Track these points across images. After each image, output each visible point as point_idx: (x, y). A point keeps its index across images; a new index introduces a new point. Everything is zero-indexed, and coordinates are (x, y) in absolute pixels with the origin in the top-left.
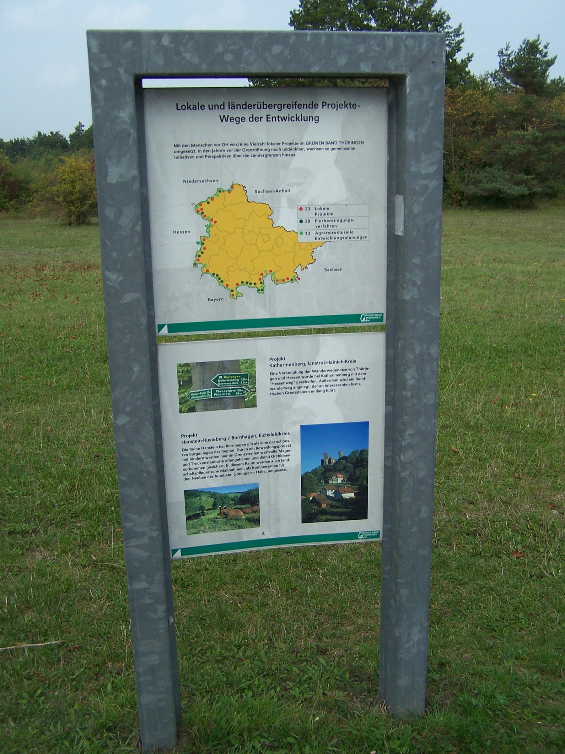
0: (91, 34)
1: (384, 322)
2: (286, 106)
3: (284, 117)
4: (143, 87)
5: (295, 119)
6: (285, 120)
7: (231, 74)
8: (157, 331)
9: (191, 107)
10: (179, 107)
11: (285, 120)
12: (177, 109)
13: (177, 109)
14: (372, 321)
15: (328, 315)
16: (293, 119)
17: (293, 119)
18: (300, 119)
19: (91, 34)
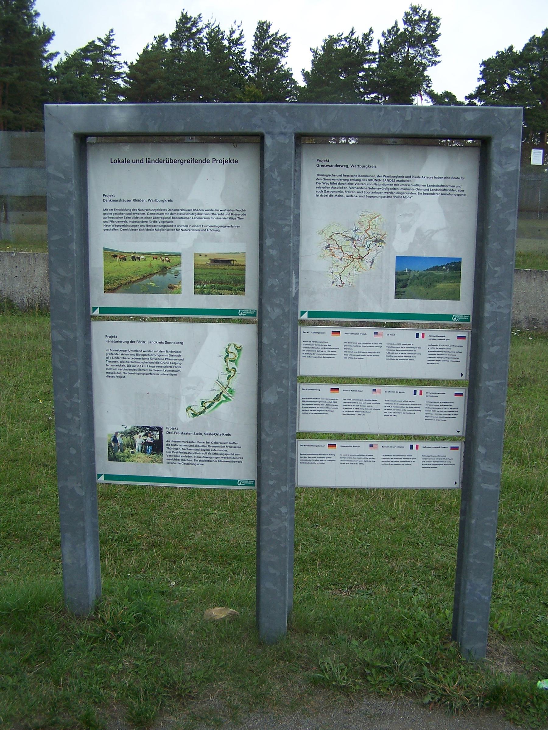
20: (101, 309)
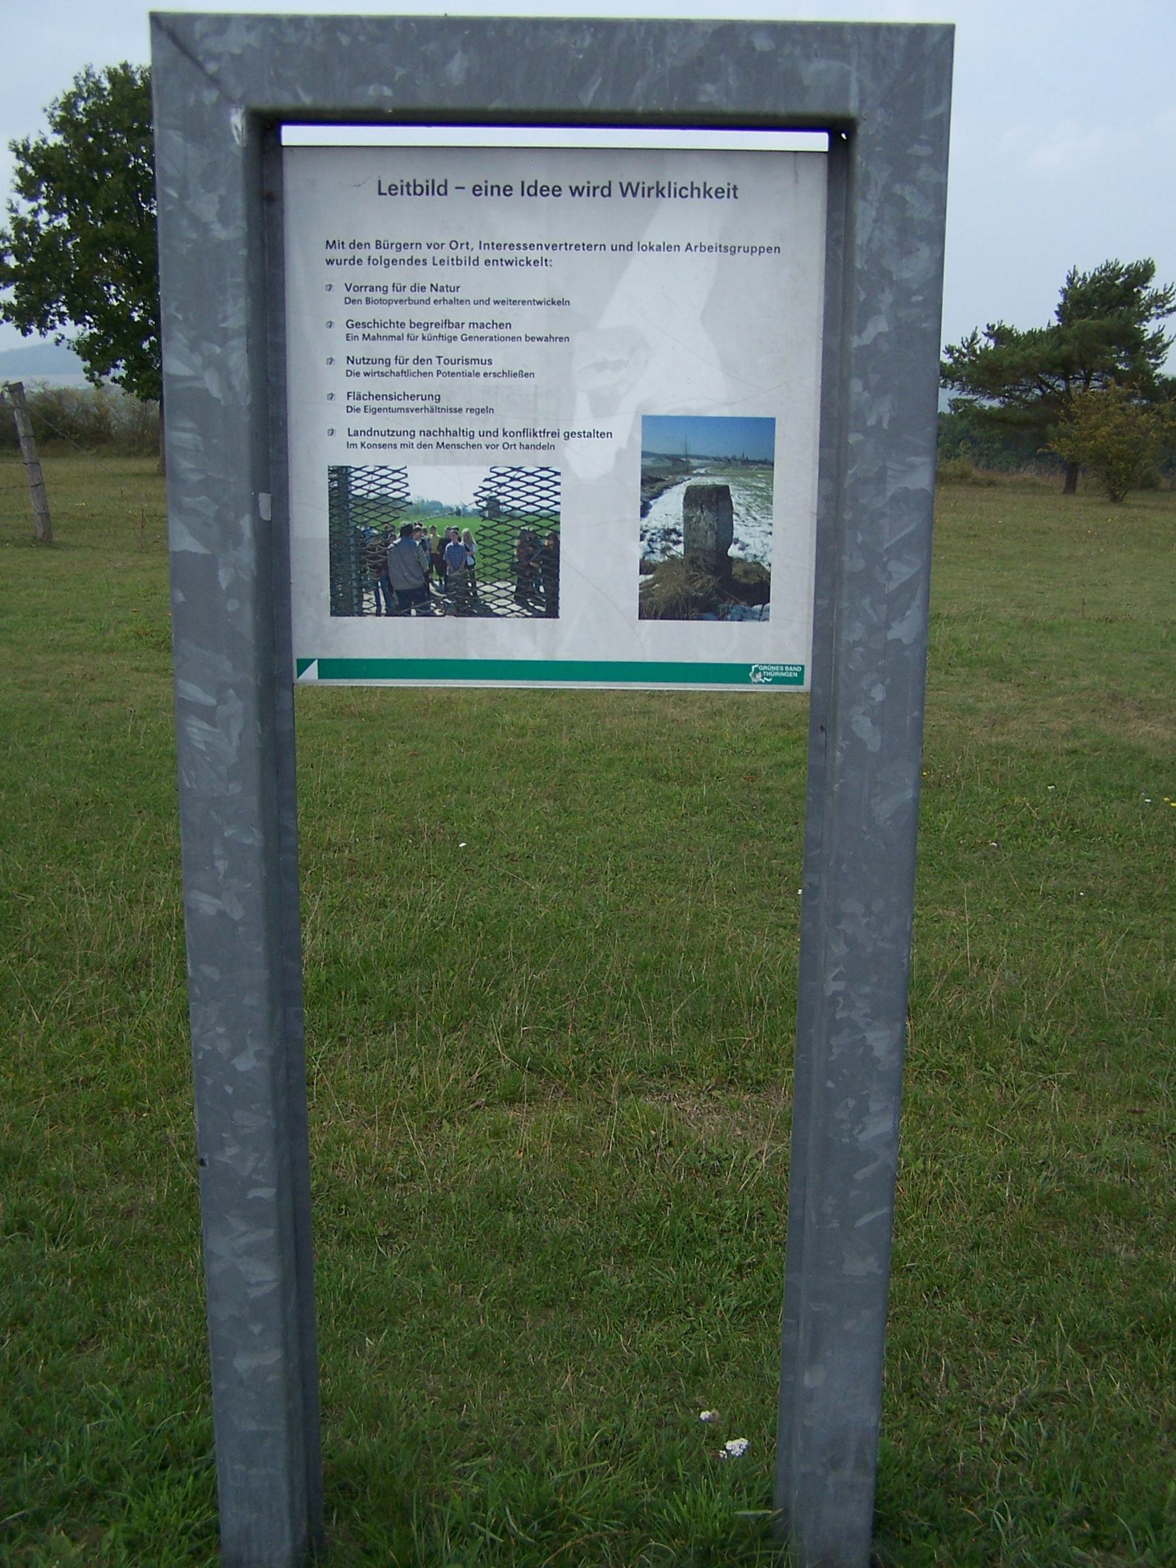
0: (948, 32)
1: (807, 686)
2: (598, 191)
3: (577, 188)
4: (284, 143)
5: (689, 192)
6: (580, 195)
7: (724, 115)
8: (295, 674)
9: (712, 193)
10: (384, 190)
11: (580, 195)
12: (380, 194)
13: (380, 194)
14: (777, 681)
15: (678, 661)
16: (684, 192)
17: (684, 192)
18: (666, 192)
19: (948, 32)
20: (322, 663)
